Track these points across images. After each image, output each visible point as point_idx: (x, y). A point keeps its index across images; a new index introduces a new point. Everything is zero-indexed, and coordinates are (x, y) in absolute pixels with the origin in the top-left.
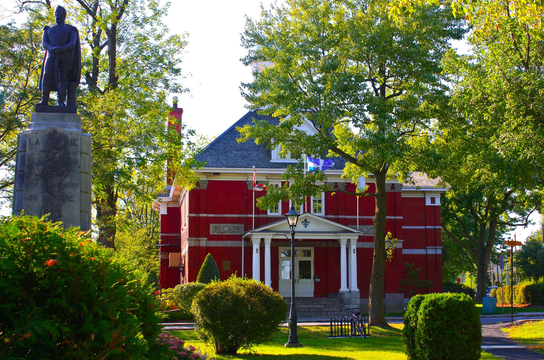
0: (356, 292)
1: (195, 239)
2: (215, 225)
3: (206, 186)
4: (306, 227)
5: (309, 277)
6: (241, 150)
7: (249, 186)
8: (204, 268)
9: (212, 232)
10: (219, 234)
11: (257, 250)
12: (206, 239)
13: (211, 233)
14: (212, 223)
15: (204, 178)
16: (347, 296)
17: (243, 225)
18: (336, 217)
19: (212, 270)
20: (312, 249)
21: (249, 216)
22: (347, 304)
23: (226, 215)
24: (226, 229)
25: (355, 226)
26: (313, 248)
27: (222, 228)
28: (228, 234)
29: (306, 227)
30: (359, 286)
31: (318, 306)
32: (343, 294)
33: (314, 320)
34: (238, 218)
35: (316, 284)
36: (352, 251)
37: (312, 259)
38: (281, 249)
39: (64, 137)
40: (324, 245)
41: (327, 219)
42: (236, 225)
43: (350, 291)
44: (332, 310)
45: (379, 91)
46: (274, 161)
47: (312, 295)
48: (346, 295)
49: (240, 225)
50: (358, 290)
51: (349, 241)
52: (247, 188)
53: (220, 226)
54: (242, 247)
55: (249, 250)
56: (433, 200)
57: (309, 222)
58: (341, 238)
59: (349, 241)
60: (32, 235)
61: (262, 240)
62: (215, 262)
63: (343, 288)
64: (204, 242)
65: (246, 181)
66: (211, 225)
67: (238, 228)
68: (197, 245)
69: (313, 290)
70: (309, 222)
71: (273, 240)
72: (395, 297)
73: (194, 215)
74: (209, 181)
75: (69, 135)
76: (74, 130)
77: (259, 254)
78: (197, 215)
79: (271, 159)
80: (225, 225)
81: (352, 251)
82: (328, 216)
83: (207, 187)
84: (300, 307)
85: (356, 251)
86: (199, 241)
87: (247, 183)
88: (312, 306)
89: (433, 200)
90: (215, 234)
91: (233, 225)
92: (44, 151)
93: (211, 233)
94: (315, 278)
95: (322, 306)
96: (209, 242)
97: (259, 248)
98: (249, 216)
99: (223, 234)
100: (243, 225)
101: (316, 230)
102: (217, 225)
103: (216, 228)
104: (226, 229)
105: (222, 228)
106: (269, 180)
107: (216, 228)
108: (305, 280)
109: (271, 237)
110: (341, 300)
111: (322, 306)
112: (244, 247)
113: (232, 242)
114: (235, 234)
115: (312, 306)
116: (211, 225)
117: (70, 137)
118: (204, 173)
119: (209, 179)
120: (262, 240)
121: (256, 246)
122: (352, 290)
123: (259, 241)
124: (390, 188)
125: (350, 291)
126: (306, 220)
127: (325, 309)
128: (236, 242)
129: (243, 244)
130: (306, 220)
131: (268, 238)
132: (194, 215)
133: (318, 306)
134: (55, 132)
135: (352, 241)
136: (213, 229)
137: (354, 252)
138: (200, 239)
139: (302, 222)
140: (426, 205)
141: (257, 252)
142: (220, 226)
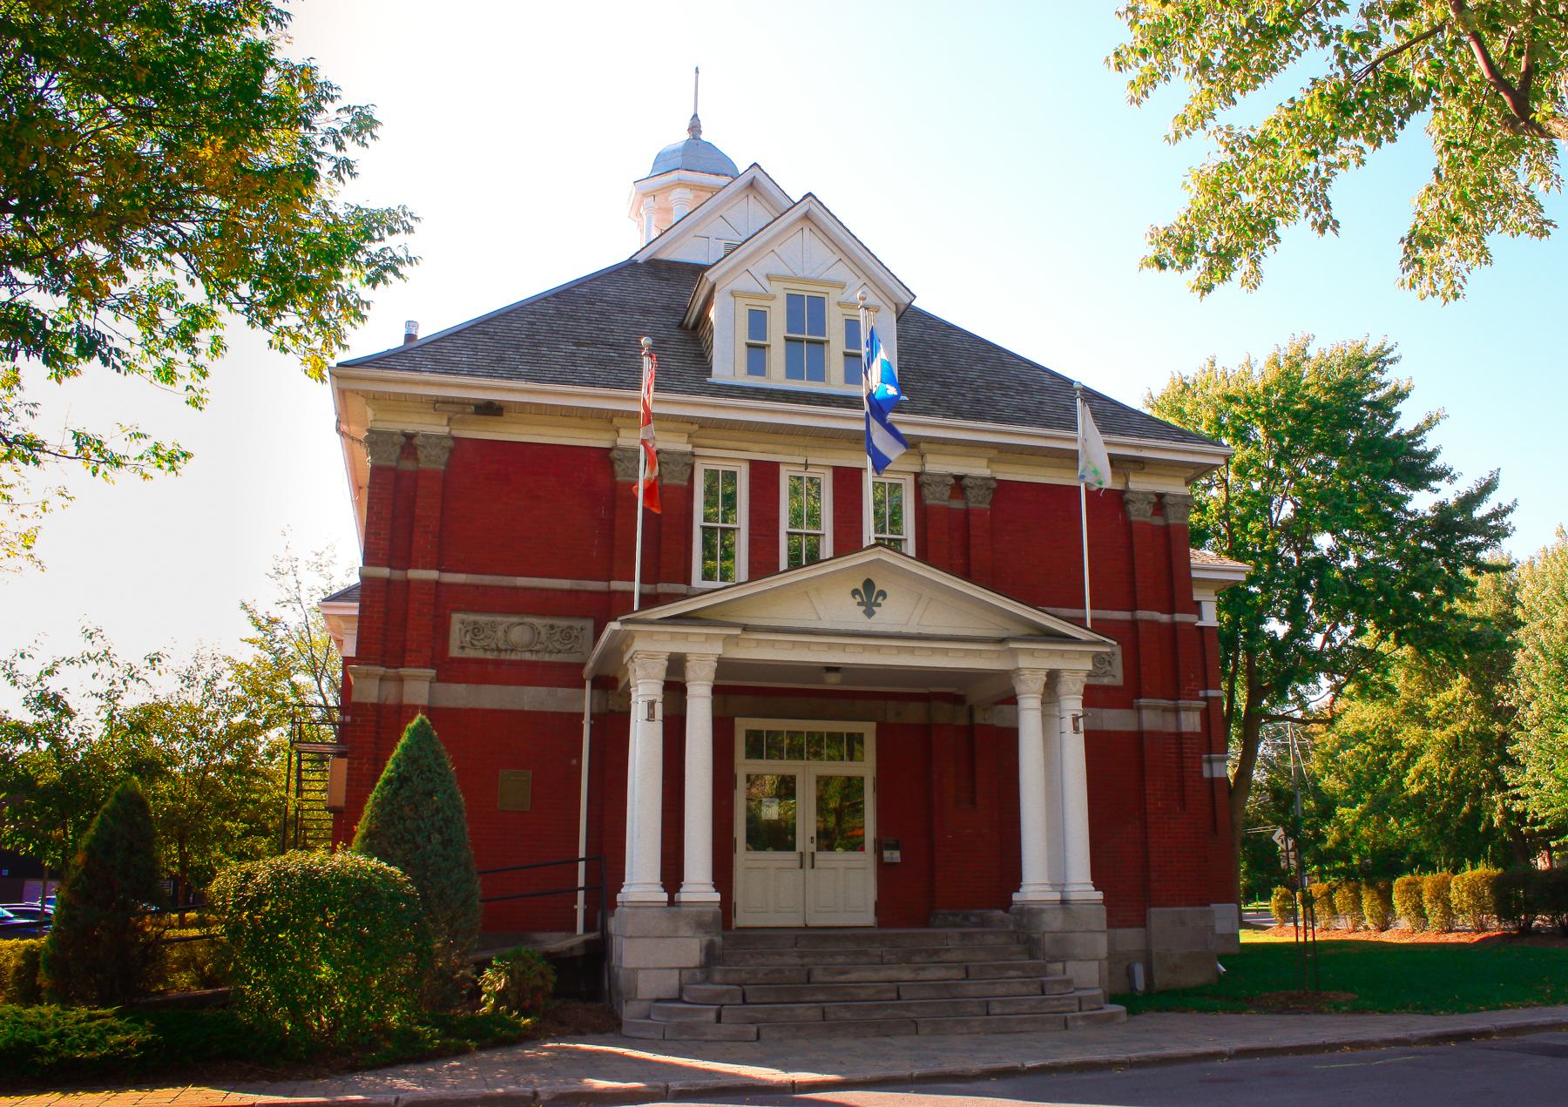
0: (1088, 902)
1: (381, 670)
2: (472, 617)
3: (445, 457)
4: (869, 613)
5: (857, 845)
6: (594, 344)
7: (618, 468)
8: (389, 781)
9: (457, 647)
10: (489, 656)
11: (651, 705)
12: (432, 672)
13: (454, 652)
14: (458, 610)
15: (432, 426)
16: (1053, 922)
19: (430, 794)
20: (868, 729)
21: (617, 585)
22: (1055, 960)
23: (522, 581)
24: (518, 635)
25: (1076, 613)
26: (874, 724)
27: (500, 634)
28: (527, 656)
29: (869, 613)
31: (932, 973)
32: (1029, 913)
33: (976, 1066)
34: (570, 592)
35: (883, 868)
37: (865, 768)
42: (563, 623)
44: (1000, 990)
46: (719, 381)
47: (869, 918)
48: (1047, 917)
49: (577, 623)
50: (1099, 895)
51: (1053, 678)
52: (613, 474)
53: (493, 626)
54: (581, 715)
55: (613, 730)
57: (883, 594)
58: (1024, 662)
59: (1053, 678)
61: (677, 664)
62: (447, 759)
63: (1035, 885)
64: (418, 687)
65: (609, 450)
66: (456, 618)
67: (567, 634)
68: (391, 700)
70: (883, 594)
72: (1183, 923)
73: (385, 572)
74: (457, 440)
77: (657, 727)
78: (398, 575)
79: (710, 375)
83: (448, 465)
84: (853, 977)
86: (400, 680)
87: (614, 454)
88: (906, 974)
90: (471, 653)
91: (549, 621)
93: (454, 652)
94: (880, 847)
96: (441, 687)
98: (617, 585)
99: (504, 656)
101: (913, 629)
102: (482, 619)
103: (476, 629)
104: (518, 635)
105: (500, 634)
106: (698, 451)
107: (476, 629)
108: (840, 856)
109: (717, 649)
110: (1026, 933)
112: (592, 716)
113: (543, 691)
114: (554, 658)
115: (906, 974)
116: (456, 618)
118: (440, 405)
119: (456, 433)
120: (677, 664)
121: (645, 691)
122: (1073, 896)
123: (659, 669)
124: (1150, 510)
125: (1064, 902)
126: (869, 584)
127: (972, 988)
128: (562, 692)
129: (586, 702)
130: (869, 584)
131: (704, 654)
132: (385, 572)
133: (932, 973)
135: (1066, 677)
137: (1076, 729)
138: (403, 671)
139: (855, 592)
141: (651, 717)
142: (493, 626)
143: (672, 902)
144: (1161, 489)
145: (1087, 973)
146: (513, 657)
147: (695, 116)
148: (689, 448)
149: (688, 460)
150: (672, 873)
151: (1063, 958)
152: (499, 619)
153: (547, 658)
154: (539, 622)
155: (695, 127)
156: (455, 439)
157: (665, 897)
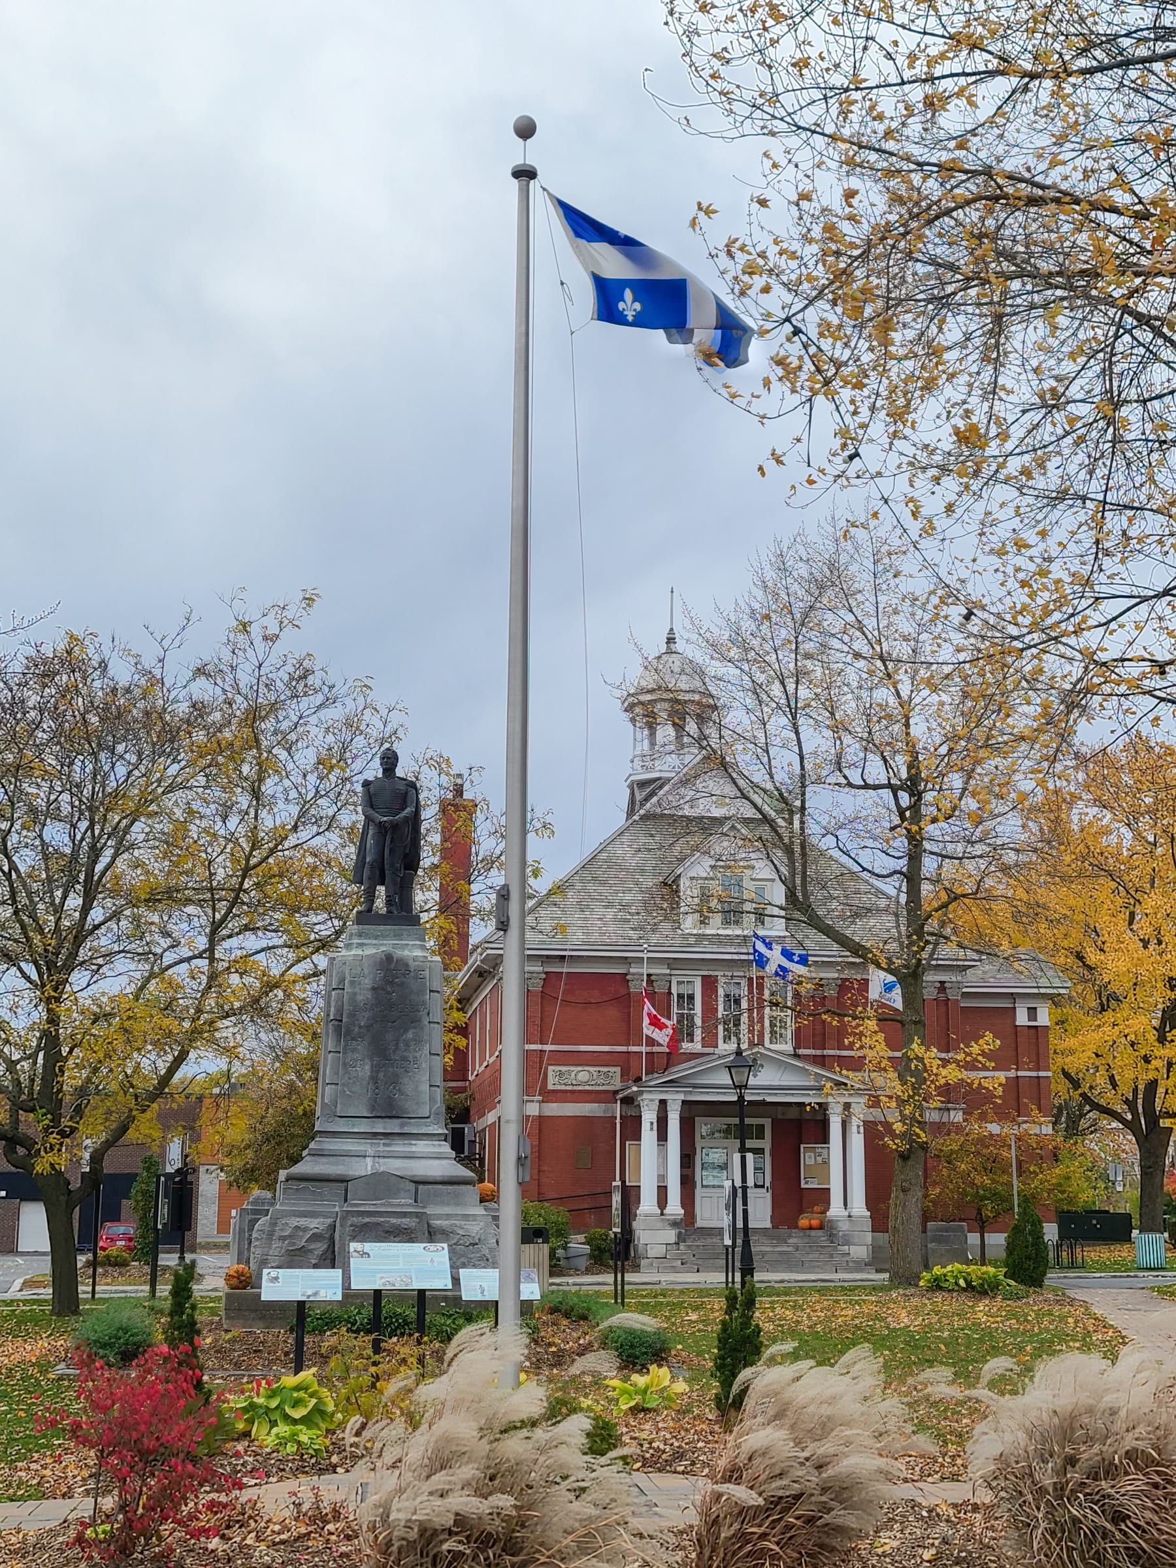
0: (862, 1217)
13: (550, 1087)
16: (844, 1226)
17: (618, 1069)
18: (819, 1052)
20: (767, 1123)
28: (587, 1088)
30: (870, 1204)
36: (854, 1129)
38: (703, 1127)
39: (403, 964)
40: (793, 1114)
41: (796, 1056)
42: (605, 1069)
43: (850, 1216)
45: (908, 814)
47: (768, 1225)
49: (612, 1069)
50: (869, 1213)
51: (847, 1106)
53: (569, 1072)
56: (1032, 1013)
60: (48, 1023)
61: (663, 1102)
66: (550, 1068)
69: (769, 1213)
70: (762, 1066)
71: (684, 1102)
75: (411, 962)
76: (418, 953)
80: (580, 1068)
81: (854, 1129)
82: (801, 1051)
85: (862, 1129)
89: (1032, 1013)
91: (598, 1069)
92: (373, 989)
93: (550, 1087)
95: (790, 1249)
97: (655, 1121)
99: (576, 1088)
100: (618, 1069)
102: (563, 1069)
103: (561, 1074)
109: (682, 1097)
111: (790, 1249)
114: (601, 1088)
117: (413, 965)
120: (663, 1102)
121: (649, 1117)
125: (850, 1216)
134: (389, 957)
136: (554, 1078)
140: (1017, 1023)
141: (652, 1129)
142: (569, 1072)
143: (662, 1214)
144: (943, 978)
145: (860, 1252)
146: (580, 1088)
147: (672, 629)
148: (668, 971)
149: (667, 978)
150: (662, 1201)
151: (847, 1243)
152: (572, 1068)
153: (597, 1088)
154: (591, 1069)
155: (670, 640)
156: (546, 973)
157: (659, 1211)
